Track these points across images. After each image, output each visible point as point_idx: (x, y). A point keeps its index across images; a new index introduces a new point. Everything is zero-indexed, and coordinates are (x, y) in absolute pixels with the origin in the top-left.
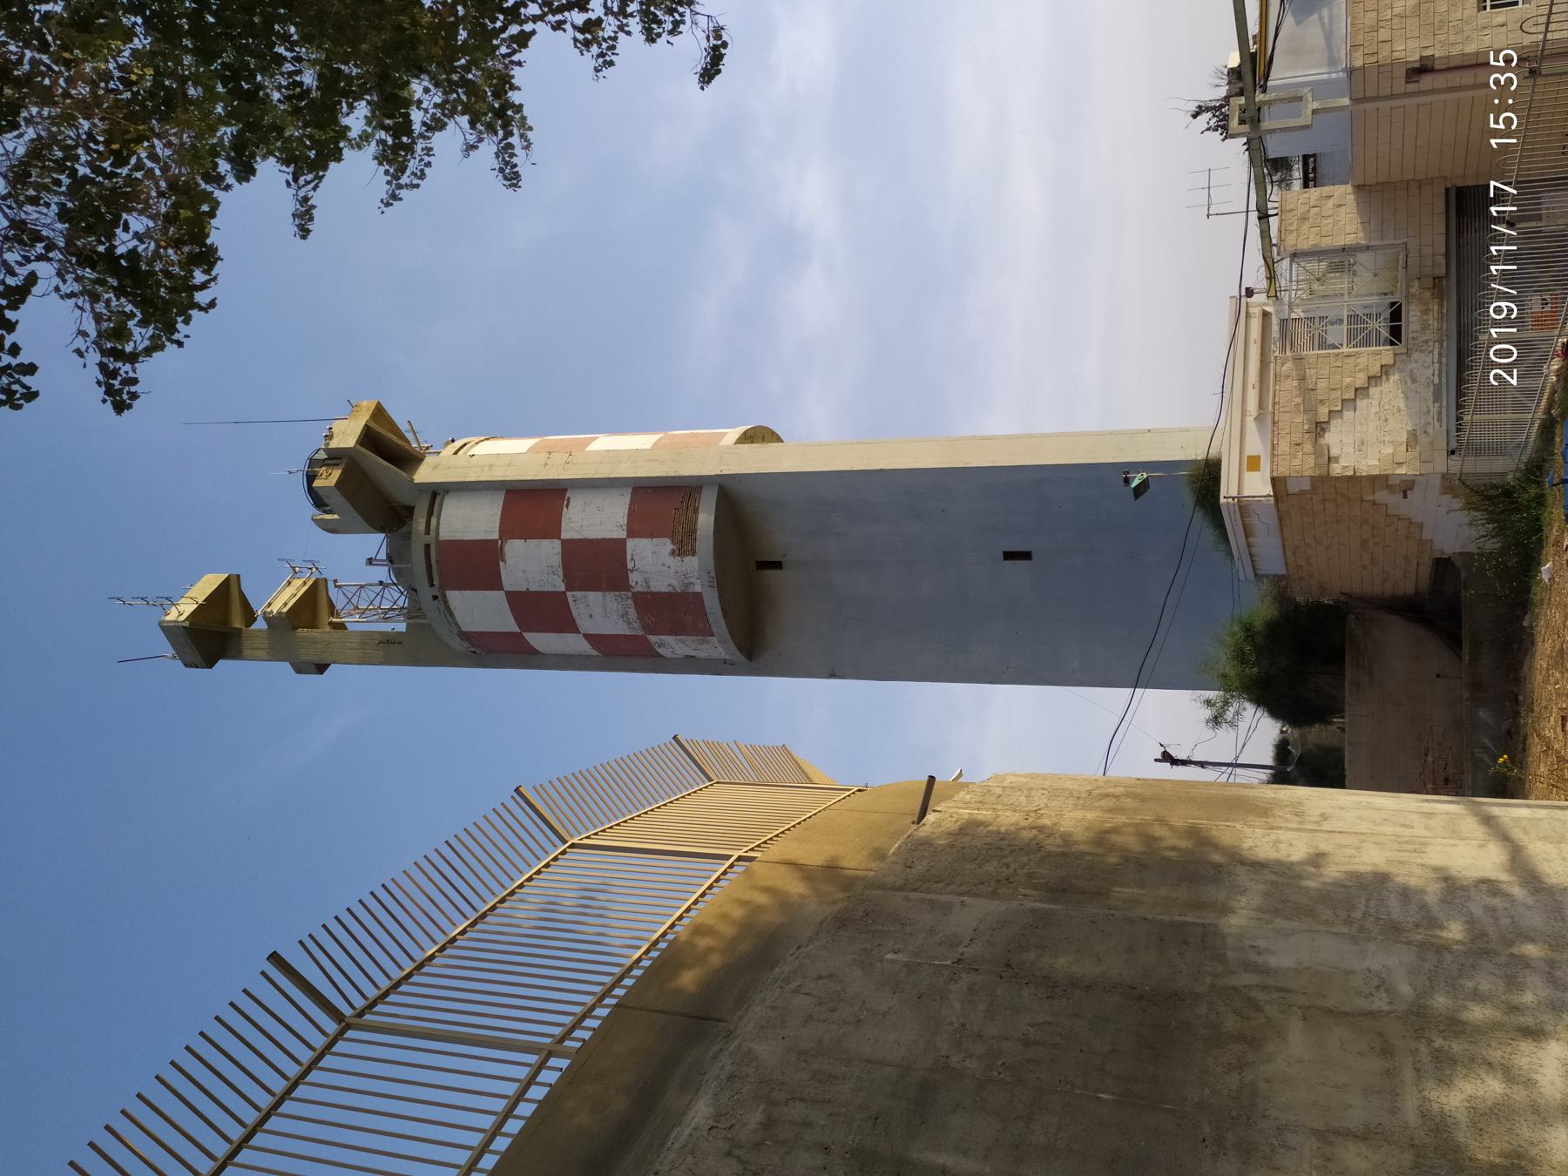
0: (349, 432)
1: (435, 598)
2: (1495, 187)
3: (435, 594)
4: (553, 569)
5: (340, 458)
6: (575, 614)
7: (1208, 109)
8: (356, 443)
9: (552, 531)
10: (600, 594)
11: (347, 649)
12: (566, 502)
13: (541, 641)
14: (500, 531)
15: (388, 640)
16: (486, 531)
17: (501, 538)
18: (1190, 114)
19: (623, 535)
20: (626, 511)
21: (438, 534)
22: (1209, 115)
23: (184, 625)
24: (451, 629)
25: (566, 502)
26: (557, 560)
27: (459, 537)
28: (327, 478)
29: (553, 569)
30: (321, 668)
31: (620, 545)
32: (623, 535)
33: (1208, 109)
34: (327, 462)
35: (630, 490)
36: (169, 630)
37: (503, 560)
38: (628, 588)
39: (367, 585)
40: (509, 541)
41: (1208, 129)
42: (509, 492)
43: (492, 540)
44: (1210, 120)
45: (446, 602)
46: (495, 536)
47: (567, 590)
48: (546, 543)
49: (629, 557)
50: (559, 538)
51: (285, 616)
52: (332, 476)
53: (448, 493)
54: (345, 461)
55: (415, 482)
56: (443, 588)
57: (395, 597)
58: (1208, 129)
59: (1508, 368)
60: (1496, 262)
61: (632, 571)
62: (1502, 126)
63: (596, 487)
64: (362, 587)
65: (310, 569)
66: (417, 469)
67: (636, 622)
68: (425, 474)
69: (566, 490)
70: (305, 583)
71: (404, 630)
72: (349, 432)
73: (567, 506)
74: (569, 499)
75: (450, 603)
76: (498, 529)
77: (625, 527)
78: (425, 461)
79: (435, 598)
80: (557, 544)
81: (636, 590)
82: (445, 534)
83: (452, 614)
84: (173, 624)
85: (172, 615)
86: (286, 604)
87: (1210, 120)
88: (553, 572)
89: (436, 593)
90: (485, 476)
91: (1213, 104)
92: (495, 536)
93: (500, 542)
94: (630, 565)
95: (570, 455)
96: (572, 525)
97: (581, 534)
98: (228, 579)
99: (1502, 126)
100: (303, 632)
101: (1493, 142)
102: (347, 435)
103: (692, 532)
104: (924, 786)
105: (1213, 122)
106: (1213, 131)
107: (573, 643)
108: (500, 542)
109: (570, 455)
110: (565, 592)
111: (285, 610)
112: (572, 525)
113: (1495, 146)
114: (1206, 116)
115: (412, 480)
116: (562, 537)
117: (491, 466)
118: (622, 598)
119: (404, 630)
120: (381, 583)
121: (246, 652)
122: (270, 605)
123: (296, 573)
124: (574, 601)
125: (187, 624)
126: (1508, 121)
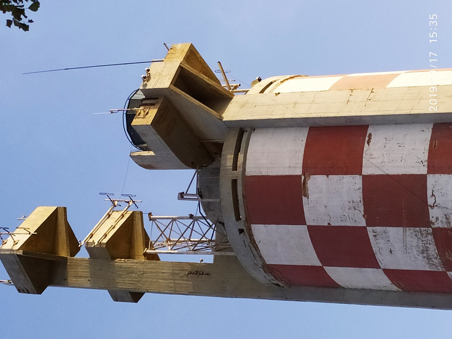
5: (157, 98)
6: (375, 249)
10: (401, 229)
11: (159, 279)
17: (304, 174)
19: (423, 170)
20: (427, 148)
21: (244, 169)
26: (358, 196)
27: (264, 173)
31: (422, 179)
32: (423, 170)
37: (306, 195)
38: (428, 224)
39: (178, 218)
42: (312, 129)
45: (251, 236)
46: (298, 172)
48: (347, 178)
49: (429, 193)
50: (360, 173)
51: (104, 246)
53: (254, 130)
54: (160, 101)
56: (250, 221)
61: (432, 207)
62: (433, 36)
64: (174, 220)
65: (128, 202)
67: (436, 258)
69: (368, 126)
70: (123, 216)
71: (212, 263)
73: (368, 143)
74: (370, 135)
76: (301, 165)
77: (426, 163)
79: (241, 231)
81: (436, 225)
83: (256, 248)
84: (9, 253)
86: (106, 235)
88: (354, 208)
92: (298, 172)
93: (303, 177)
94: (430, 201)
100: (120, 262)
101: (430, 41)
108: (303, 177)
111: (105, 241)
115: (221, 119)
116: (363, 173)
117: (295, 103)
118: (422, 235)
120: (191, 216)
121: (71, 280)
122: (92, 236)
125: (20, 253)
126: (434, 35)
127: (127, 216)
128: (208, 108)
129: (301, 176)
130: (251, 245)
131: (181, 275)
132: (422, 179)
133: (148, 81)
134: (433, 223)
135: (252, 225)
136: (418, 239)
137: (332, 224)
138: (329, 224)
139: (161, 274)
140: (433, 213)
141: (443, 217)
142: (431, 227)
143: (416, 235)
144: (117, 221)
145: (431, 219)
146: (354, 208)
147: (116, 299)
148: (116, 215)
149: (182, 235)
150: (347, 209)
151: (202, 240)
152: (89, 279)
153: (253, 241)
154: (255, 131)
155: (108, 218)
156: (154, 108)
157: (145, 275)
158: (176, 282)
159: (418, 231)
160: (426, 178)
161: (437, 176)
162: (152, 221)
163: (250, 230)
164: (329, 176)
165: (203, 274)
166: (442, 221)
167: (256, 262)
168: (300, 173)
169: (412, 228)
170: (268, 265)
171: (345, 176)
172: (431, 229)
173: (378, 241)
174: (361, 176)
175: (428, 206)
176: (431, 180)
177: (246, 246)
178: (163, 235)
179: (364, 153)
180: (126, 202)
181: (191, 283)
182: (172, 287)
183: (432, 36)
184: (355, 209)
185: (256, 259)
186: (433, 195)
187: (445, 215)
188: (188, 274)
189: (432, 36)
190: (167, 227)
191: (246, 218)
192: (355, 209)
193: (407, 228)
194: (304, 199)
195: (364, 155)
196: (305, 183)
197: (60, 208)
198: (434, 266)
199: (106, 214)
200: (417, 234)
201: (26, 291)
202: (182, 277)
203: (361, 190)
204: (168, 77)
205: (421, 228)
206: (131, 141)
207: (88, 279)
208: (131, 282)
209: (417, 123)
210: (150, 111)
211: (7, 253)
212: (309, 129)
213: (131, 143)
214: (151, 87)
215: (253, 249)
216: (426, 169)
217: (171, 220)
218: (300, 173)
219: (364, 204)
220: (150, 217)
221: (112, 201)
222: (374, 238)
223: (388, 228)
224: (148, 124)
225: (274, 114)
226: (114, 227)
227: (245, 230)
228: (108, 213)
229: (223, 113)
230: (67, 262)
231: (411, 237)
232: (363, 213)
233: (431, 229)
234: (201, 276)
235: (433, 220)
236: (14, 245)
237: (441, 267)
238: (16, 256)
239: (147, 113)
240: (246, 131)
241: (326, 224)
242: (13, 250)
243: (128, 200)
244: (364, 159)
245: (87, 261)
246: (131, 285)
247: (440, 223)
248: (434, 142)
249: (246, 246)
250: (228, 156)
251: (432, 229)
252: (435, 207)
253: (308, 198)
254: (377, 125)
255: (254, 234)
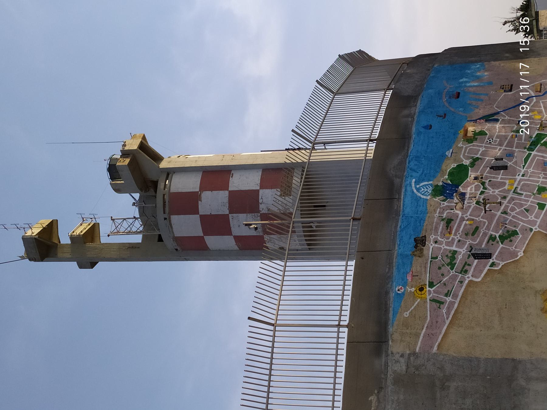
0: (133, 144)
1: (165, 219)
2: (521, 65)
3: (166, 217)
4: (224, 204)
5: (129, 155)
6: (231, 225)
7: (509, 22)
8: (138, 147)
9: (225, 187)
10: (245, 215)
11: (111, 251)
12: (231, 175)
13: (212, 241)
14: (200, 188)
15: (132, 247)
16: (193, 188)
17: (200, 191)
18: (502, 23)
19: (258, 188)
20: (260, 178)
21: (170, 190)
22: (510, 23)
23: (35, 237)
24: (170, 235)
25: (231, 175)
26: (226, 200)
27: (180, 191)
28: (123, 162)
29: (224, 204)
30: (92, 265)
31: (258, 191)
32: (258, 188)
33: (509, 22)
34: (122, 156)
35: (262, 170)
36: (26, 240)
37: (201, 201)
38: (258, 211)
39: (127, 219)
40: (204, 192)
41: (509, 31)
42: (204, 172)
43: (196, 192)
44: (510, 25)
45: (170, 221)
46: (198, 190)
47: (229, 213)
48: (221, 192)
49: (260, 197)
50: (228, 190)
51: (82, 236)
52: (125, 161)
53: (175, 173)
54: (131, 156)
55: (160, 167)
56: (171, 213)
57: (138, 225)
58: (509, 31)
59: (526, 129)
60: (521, 70)
61: (261, 204)
62: (524, 44)
63: (245, 169)
64: (125, 219)
65: (92, 219)
66: (160, 163)
67: (260, 228)
68: (163, 165)
69: (231, 171)
70: (89, 224)
71: (141, 242)
72: (133, 144)
73: (232, 177)
74: (233, 174)
75: (172, 222)
76: (199, 187)
77: (259, 185)
78: (164, 160)
79: (165, 219)
80: (227, 193)
81: (262, 212)
82: (173, 189)
83: (172, 227)
84: (30, 237)
85: (29, 233)
86: (82, 232)
87: (510, 25)
88: (224, 205)
89: (167, 217)
90: (193, 165)
91: (511, 20)
92: (198, 190)
93: (199, 192)
94: (260, 201)
95: (233, 156)
96: (234, 184)
97: (239, 189)
98: (52, 222)
99: (524, 44)
100: (89, 245)
101: (521, 49)
102: (133, 145)
103: (290, 187)
104: (531, 96)
105: (512, 28)
106: (511, 31)
107: (228, 242)
108: (199, 192)
109: (233, 156)
110: (228, 215)
111: (82, 234)
112: (234, 184)
113: (522, 95)
114: (508, 24)
115: (159, 167)
116: (229, 190)
117: (196, 161)
118: (255, 217)
119: (141, 242)
120: (135, 217)
121: (60, 255)
122: (73, 232)
123: (84, 220)
124: (233, 218)
125: (37, 237)
127: (92, 224)
128: (154, 162)
129: (198, 192)
130: (169, 226)
131: (124, 249)
132: (258, 191)
133: (125, 147)
134: (261, 211)
135: (171, 216)
136: (253, 219)
137: (212, 214)
138: (211, 214)
139: (113, 249)
140: (261, 207)
141: (265, 208)
142: (260, 213)
143: (252, 217)
144: (87, 226)
145: (260, 209)
146: (224, 205)
147: (81, 267)
148: (85, 225)
149: (129, 226)
150: (220, 206)
151: (137, 231)
152: (71, 253)
153: (171, 224)
154: (175, 173)
155: (81, 225)
156: (128, 158)
157: (103, 250)
158: (121, 252)
159: (253, 215)
160: (259, 191)
161: (264, 190)
162: (112, 221)
163: (170, 218)
164: (213, 191)
165: (136, 248)
166: (265, 210)
167: (170, 235)
168: (198, 191)
169: (251, 214)
170: (175, 237)
171: (220, 191)
172: (259, 214)
173: (234, 221)
174: (228, 191)
175: (259, 203)
176: (261, 192)
177: (166, 227)
178: (116, 226)
179: (230, 181)
180: (91, 218)
181: (129, 252)
182: (118, 255)
183: (523, 43)
184: (224, 206)
185: (170, 233)
186: (262, 198)
187: (267, 207)
188: (128, 248)
189: (523, 43)
190: (119, 224)
191: (169, 212)
192: (224, 206)
193: (249, 214)
194: (199, 202)
195: (230, 182)
196: (200, 195)
197: (54, 220)
198: (258, 233)
199: (73, 231)
200: (253, 216)
201: (34, 259)
202: (124, 250)
203: (228, 197)
204: (136, 145)
205: (255, 214)
206: (109, 178)
207: (69, 253)
208: (95, 254)
209: (254, 169)
210: (126, 160)
211: (28, 237)
212: (202, 173)
213: (109, 179)
214: (127, 149)
215: (170, 228)
216: (259, 187)
217: (123, 220)
218: (198, 191)
219: (229, 204)
220: (111, 218)
221: (82, 218)
222: (232, 220)
223: (239, 214)
224: (126, 164)
225: (186, 165)
226: (85, 229)
227: (167, 219)
228: (81, 223)
229: (160, 164)
230: (57, 246)
231: (250, 218)
232: (228, 208)
233: (259, 214)
234: (135, 249)
235: (261, 209)
236: (32, 234)
237: (262, 233)
238: (34, 239)
239: (125, 160)
240: (171, 173)
241: (209, 214)
242: (32, 236)
243: (92, 217)
244: (230, 184)
245: (69, 245)
246: (95, 255)
247: (264, 211)
248: (263, 176)
249: (166, 227)
250: (162, 184)
251: (260, 214)
252: (262, 204)
253: (201, 202)
254: (236, 170)
255: (171, 220)
